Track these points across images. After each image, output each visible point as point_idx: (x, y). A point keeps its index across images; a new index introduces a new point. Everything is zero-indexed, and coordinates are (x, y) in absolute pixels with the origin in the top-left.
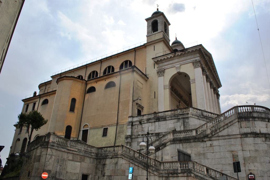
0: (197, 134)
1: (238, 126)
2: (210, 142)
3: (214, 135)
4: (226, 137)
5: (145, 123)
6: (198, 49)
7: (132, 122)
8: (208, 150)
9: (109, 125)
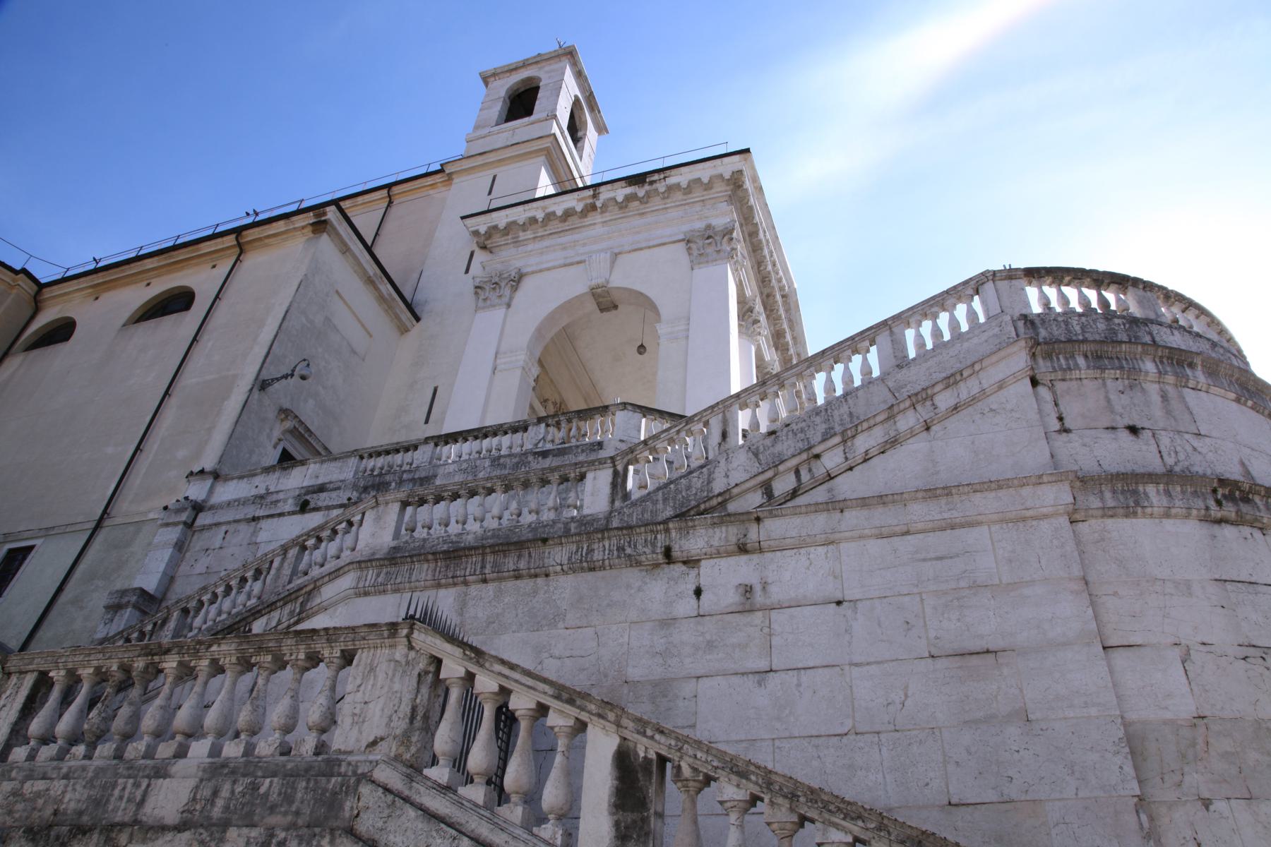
0: (618, 504)
1: (1033, 415)
2: (742, 569)
3: (794, 494)
4: (919, 512)
5: (281, 515)
6: (727, 176)
7: (198, 508)
8: (710, 645)
9: (47, 532)
